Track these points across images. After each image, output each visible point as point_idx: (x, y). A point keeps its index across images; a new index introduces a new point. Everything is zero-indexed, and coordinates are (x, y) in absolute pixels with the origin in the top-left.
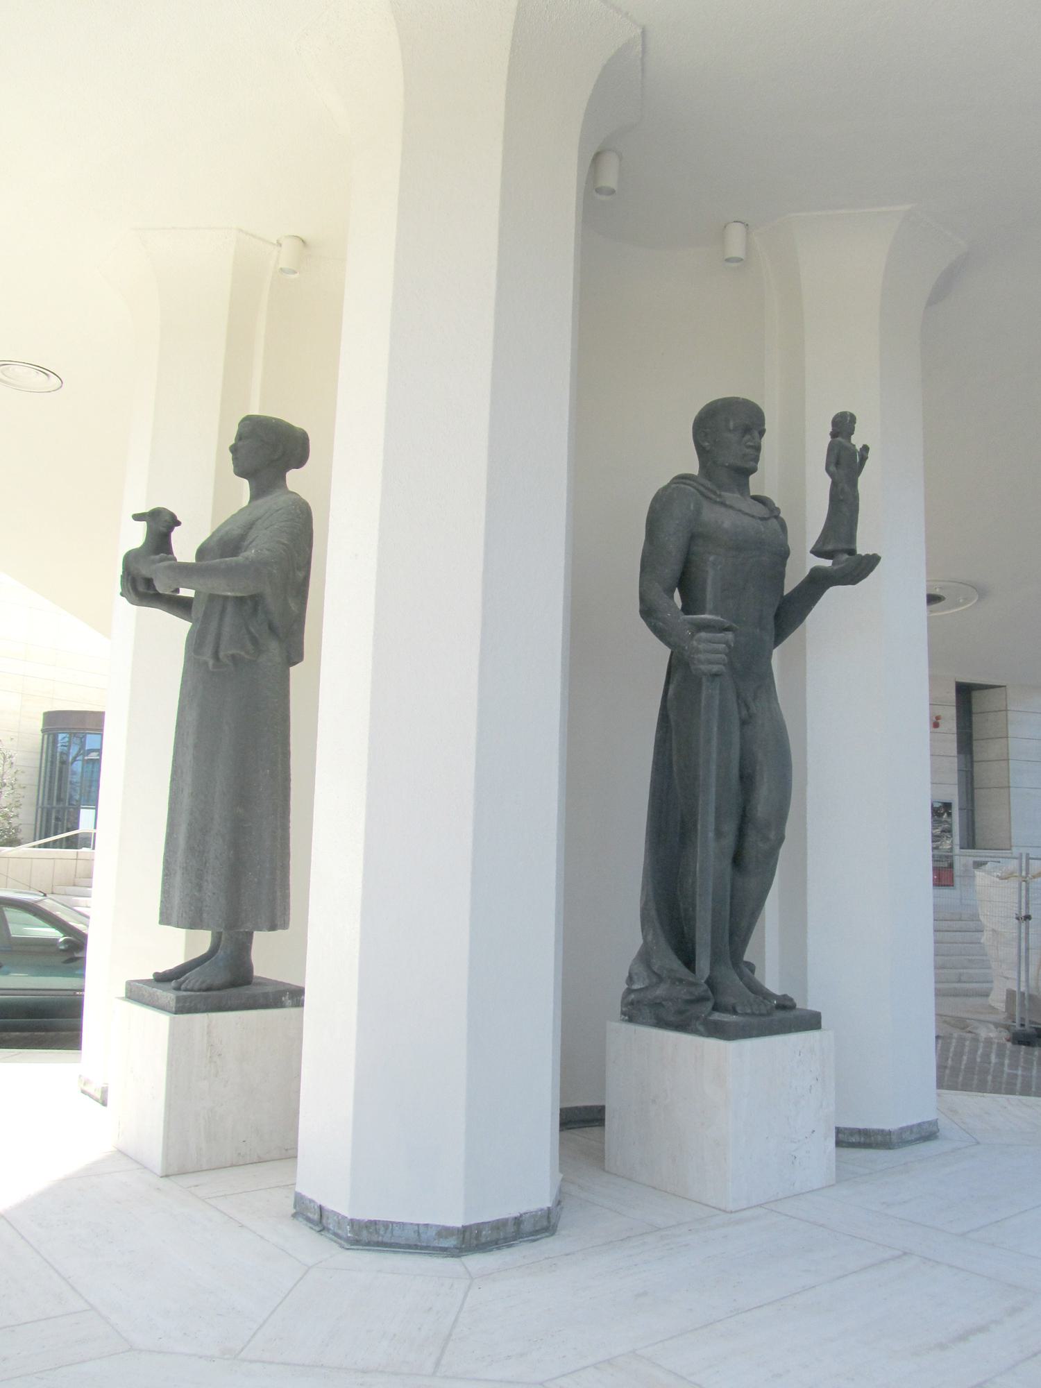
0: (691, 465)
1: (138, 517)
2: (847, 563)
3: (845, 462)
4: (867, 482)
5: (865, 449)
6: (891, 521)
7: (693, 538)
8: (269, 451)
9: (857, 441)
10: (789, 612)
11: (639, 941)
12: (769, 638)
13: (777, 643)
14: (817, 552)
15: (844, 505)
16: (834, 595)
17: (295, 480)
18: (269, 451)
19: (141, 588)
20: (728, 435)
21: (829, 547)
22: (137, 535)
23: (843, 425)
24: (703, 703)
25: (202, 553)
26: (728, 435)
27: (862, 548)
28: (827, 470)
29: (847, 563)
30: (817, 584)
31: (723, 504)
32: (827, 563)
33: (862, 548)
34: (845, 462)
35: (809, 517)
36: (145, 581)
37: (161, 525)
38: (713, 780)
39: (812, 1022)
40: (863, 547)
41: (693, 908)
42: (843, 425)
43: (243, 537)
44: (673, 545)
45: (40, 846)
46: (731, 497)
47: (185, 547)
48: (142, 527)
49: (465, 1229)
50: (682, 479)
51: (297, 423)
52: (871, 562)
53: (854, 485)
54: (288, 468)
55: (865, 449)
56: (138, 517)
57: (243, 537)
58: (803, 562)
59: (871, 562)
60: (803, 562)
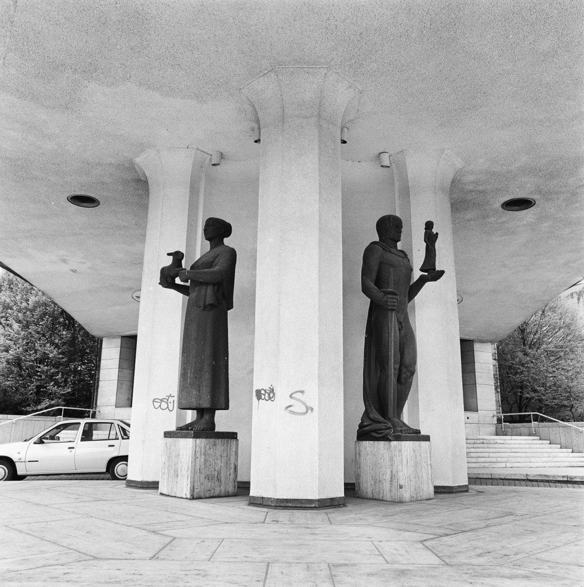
0: (376, 238)
1: (169, 254)
2: (432, 273)
3: (431, 238)
4: (437, 245)
5: (437, 234)
7: (381, 263)
8: (217, 230)
9: (434, 231)
11: (363, 409)
12: (407, 300)
13: (409, 302)
14: (421, 270)
15: (430, 253)
16: (429, 285)
17: (227, 241)
18: (217, 230)
19: (169, 280)
20: (390, 228)
21: (425, 268)
23: (429, 225)
24: (189, 478)
25: (192, 267)
26: (390, 228)
27: (438, 268)
28: (425, 241)
30: (422, 281)
31: (391, 252)
33: (438, 268)
34: (431, 238)
35: (418, 259)
36: (167, 279)
37: (178, 257)
38: (393, 348)
40: (438, 268)
42: (429, 225)
43: (213, 262)
44: (375, 268)
45: (34, 415)
46: (393, 250)
50: (374, 243)
51: (228, 221)
55: (437, 234)
56: (169, 254)
57: (213, 262)
58: (417, 274)
60: (417, 274)
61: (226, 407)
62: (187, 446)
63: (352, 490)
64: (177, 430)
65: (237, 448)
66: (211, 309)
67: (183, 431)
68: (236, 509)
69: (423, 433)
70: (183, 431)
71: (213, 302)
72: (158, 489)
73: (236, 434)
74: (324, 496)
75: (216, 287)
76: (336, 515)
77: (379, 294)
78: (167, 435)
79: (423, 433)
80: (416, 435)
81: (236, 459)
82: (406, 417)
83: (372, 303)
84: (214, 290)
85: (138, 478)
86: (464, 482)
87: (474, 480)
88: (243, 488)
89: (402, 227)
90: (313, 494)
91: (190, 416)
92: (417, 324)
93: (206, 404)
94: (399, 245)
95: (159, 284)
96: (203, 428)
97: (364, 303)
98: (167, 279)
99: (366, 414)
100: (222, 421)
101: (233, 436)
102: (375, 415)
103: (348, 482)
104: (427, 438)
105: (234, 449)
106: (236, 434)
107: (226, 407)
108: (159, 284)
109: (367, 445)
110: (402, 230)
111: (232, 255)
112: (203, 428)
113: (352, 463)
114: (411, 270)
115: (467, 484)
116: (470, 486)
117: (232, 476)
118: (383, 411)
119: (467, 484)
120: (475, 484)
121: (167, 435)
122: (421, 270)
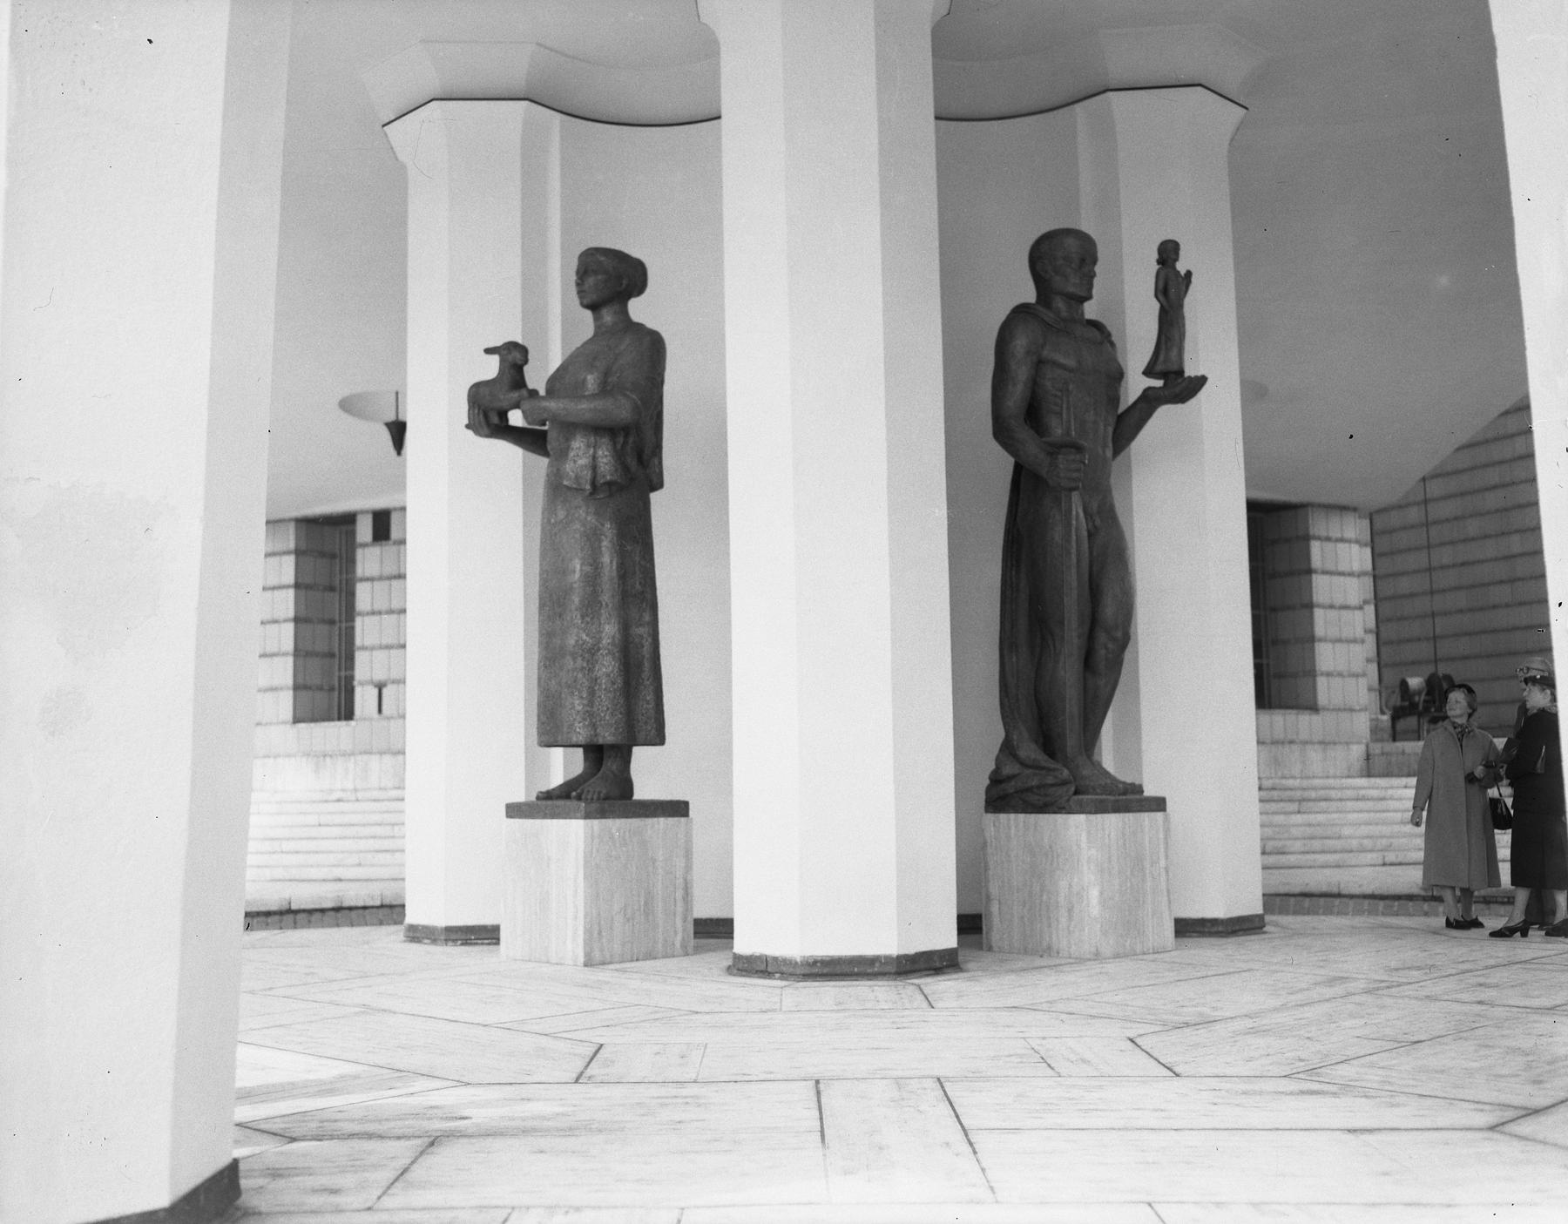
0: (1029, 294)
1: (488, 351)
2: (1176, 384)
3: (1172, 287)
5: (1189, 274)
6: (1212, 348)
8: (611, 280)
9: (1181, 267)
10: (1128, 425)
12: (1109, 453)
14: (1149, 372)
16: (1164, 413)
17: (640, 309)
18: (611, 280)
19: (495, 420)
22: (490, 368)
23: (1168, 253)
26: (1063, 262)
27: (1190, 371)
29: (1176, 384)
30: (1149, 402)
32: (1159, 383)
33: (1190, 371)
34: (1172, 287)
36: (488, 413)
37: (514, 357)
38: (1075, 584)
39: (399, 453)
41: (1045, 696)
42: (1168, 253)
47: (537, 377)
48: (495, 360)
49: (899, 957)
50: (1021, 311)
51: (635, 253)
52: (1202, 381)
53: (1007, 731)
54: (629, 297)
55: (1189, 274)
56: (488, 351)
58: (1136, 384)
59: (1202, 381)
60: (1136, 384)
61: (659, 739)
62: (571, 835)
63: (970, 925)
64: (538, 798)
65: (1167, 831)
66: (611, 495)
67: (553, 802)
68: (701, 983)
69: (1149, 791)
70: (553, 802)
71: (615, 478)
72: (498, 943)
73: (686, 804)
74: (912, 950)
75: (621, 439)
76: (942, 986)
77: (1033, 448)
78: (514, 811)
79: (1149, 791)
80: (1129, 798)
81: (688, 868)
82: (1108, 756)
83: (1018, 469)
84: (615, 450)
85: (440, 920)
86: (1256, 908)
87: (1277, 901)
88: (716, 930)
89: (1095, 261)
90: (889, 944)
91: (561, 765)
92: (1138, 525)
93: (607, 737)
94: (1090, 310)
95: (468, 427)
96: (602, 786)
97: (1001, 465)
98: (488, 413)
99: (1008, 748)
100: (650, 773)
101: (678, 809)
102: (1029, 750)
103: (671, 821)
104: (1159, 804)
105: (1404, 840)
106: (686, 804)
107: (659, 739)
108: (468, 427)
109: (1014, 823)
110: (1097, 269)
111: (653, 347)
112: (602, 786)
113: (973, 869)
114: (1118, 375)
115: (1260, 911)
116: (1268, 918)
117: (680, 909)
118: (1049, 743)
119: (1260, 911)
120: (1283, 911)
121: (514, 811)
122: (1149, 372)
